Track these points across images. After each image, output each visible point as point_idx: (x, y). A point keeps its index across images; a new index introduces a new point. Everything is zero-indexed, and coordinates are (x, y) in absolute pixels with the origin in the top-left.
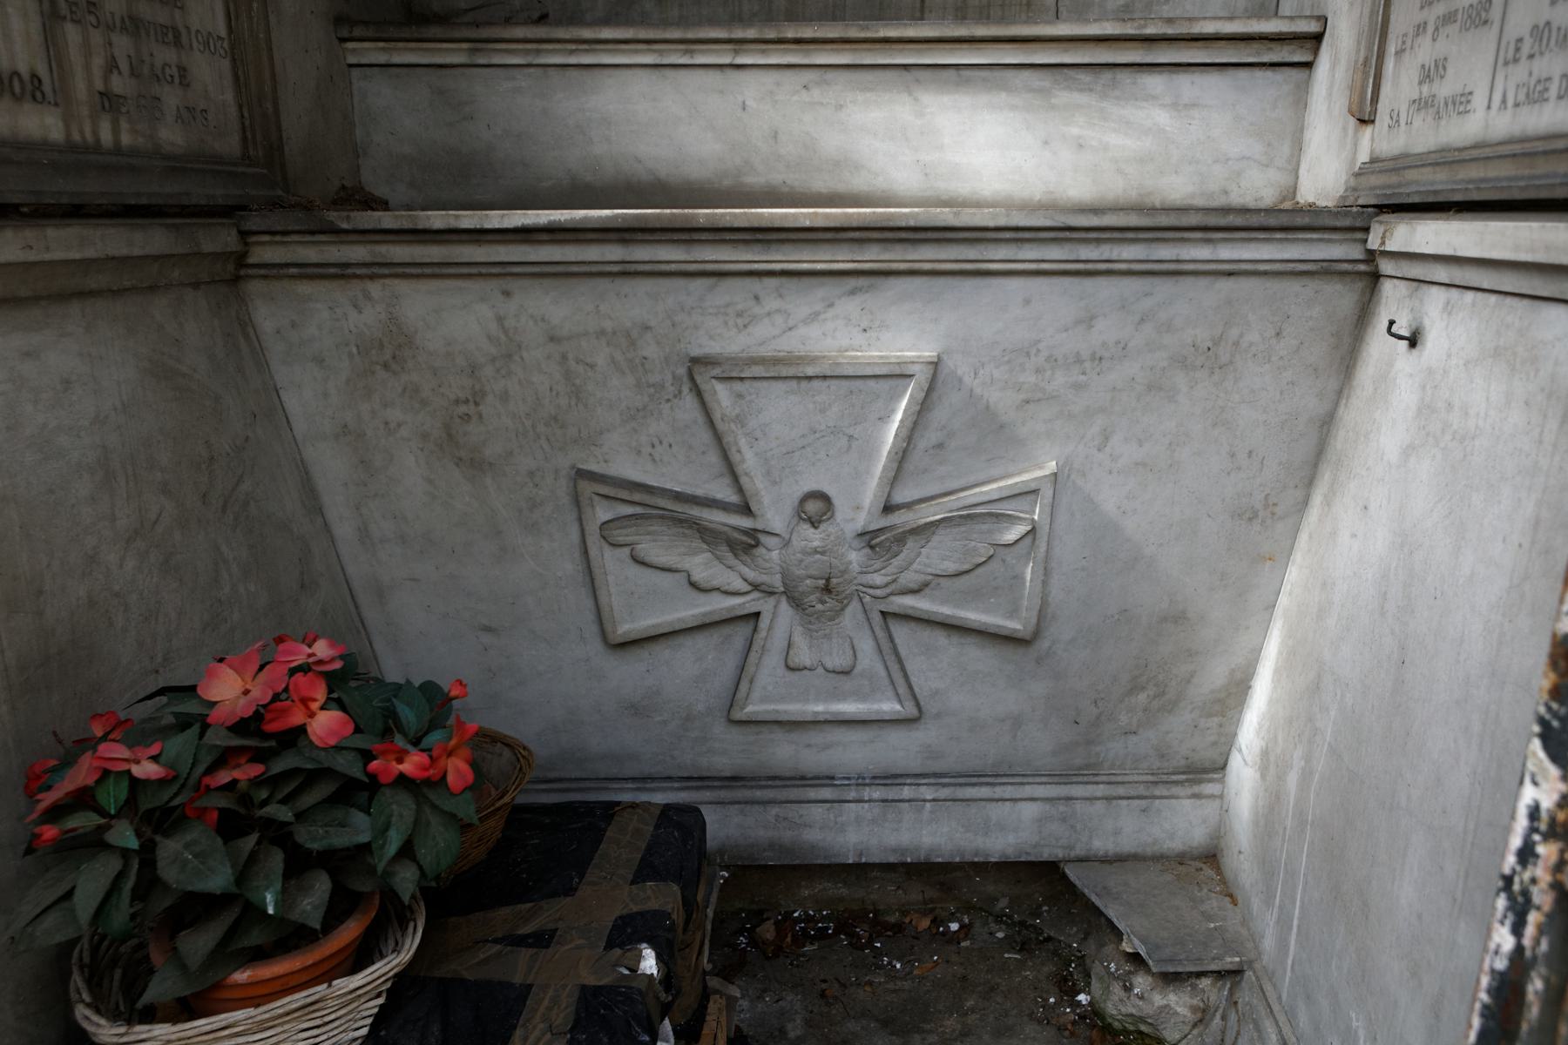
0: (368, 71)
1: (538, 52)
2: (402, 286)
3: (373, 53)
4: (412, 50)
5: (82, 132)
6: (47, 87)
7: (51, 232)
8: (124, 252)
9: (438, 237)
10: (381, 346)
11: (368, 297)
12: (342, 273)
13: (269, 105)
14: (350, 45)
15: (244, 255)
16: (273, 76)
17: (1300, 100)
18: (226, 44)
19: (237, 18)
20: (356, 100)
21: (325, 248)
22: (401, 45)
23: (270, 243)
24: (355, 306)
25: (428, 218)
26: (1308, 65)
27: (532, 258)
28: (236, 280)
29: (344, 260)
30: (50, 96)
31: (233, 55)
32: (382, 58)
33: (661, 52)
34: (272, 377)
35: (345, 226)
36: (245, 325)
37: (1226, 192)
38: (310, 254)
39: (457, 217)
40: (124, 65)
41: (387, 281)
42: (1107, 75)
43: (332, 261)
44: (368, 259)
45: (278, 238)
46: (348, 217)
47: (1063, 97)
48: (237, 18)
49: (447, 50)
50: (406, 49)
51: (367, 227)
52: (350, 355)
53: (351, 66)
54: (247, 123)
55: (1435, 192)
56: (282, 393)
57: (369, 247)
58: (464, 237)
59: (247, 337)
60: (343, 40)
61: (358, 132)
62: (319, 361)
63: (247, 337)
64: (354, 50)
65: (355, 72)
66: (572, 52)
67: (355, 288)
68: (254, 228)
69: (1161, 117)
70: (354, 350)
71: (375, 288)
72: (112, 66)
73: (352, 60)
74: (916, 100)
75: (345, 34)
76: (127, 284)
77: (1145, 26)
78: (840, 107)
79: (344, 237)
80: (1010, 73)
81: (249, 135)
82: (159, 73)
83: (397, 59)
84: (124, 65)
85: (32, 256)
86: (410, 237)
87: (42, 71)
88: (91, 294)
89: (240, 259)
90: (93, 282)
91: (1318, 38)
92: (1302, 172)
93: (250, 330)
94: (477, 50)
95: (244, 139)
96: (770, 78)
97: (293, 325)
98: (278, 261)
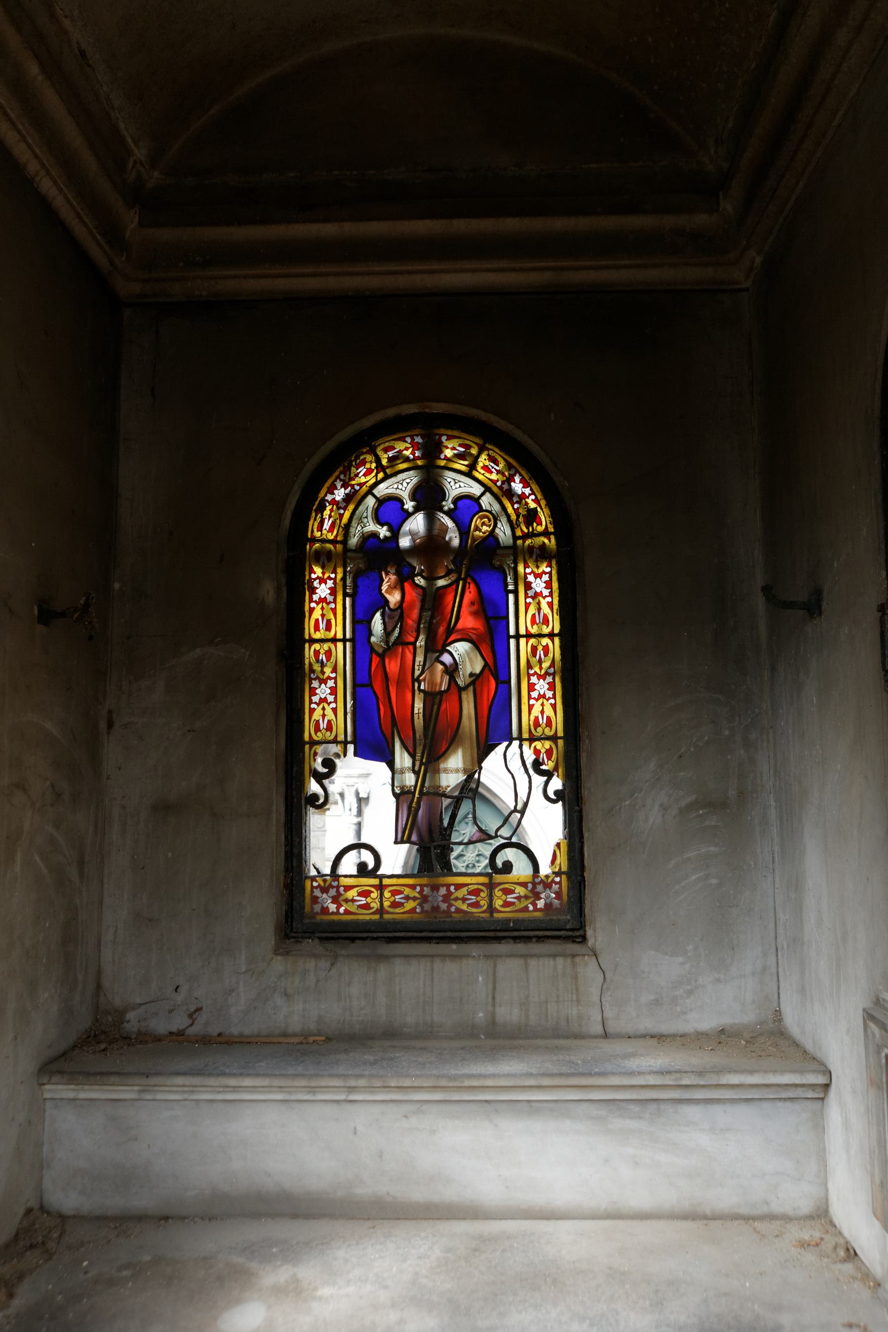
1: (192, 1092)
4: (94, 1090)
14: (47, 1087)
17: (819, 1125)
20: (47, 1123)
26: (822, 1099)
28: (799, 1180)
33: (289, 1093)
37: (767, 1203)
42: (653, 1107)
47: (618, 1123)
49: (122, 1091)
50: (90, 1090)
55: (454, 957)
60: (44, 1084)
61: (46, 1149)
64: (50, 1090)
66: (219, 1092)
69: (703, 1140)
73: (47, 1095)
74: (496, 1126)
77: (681, 1079)
78: (433, 1132)
80: (571, 1106)
91: (827, 1086)
92: (830, 1186)
96: (376, 1109)
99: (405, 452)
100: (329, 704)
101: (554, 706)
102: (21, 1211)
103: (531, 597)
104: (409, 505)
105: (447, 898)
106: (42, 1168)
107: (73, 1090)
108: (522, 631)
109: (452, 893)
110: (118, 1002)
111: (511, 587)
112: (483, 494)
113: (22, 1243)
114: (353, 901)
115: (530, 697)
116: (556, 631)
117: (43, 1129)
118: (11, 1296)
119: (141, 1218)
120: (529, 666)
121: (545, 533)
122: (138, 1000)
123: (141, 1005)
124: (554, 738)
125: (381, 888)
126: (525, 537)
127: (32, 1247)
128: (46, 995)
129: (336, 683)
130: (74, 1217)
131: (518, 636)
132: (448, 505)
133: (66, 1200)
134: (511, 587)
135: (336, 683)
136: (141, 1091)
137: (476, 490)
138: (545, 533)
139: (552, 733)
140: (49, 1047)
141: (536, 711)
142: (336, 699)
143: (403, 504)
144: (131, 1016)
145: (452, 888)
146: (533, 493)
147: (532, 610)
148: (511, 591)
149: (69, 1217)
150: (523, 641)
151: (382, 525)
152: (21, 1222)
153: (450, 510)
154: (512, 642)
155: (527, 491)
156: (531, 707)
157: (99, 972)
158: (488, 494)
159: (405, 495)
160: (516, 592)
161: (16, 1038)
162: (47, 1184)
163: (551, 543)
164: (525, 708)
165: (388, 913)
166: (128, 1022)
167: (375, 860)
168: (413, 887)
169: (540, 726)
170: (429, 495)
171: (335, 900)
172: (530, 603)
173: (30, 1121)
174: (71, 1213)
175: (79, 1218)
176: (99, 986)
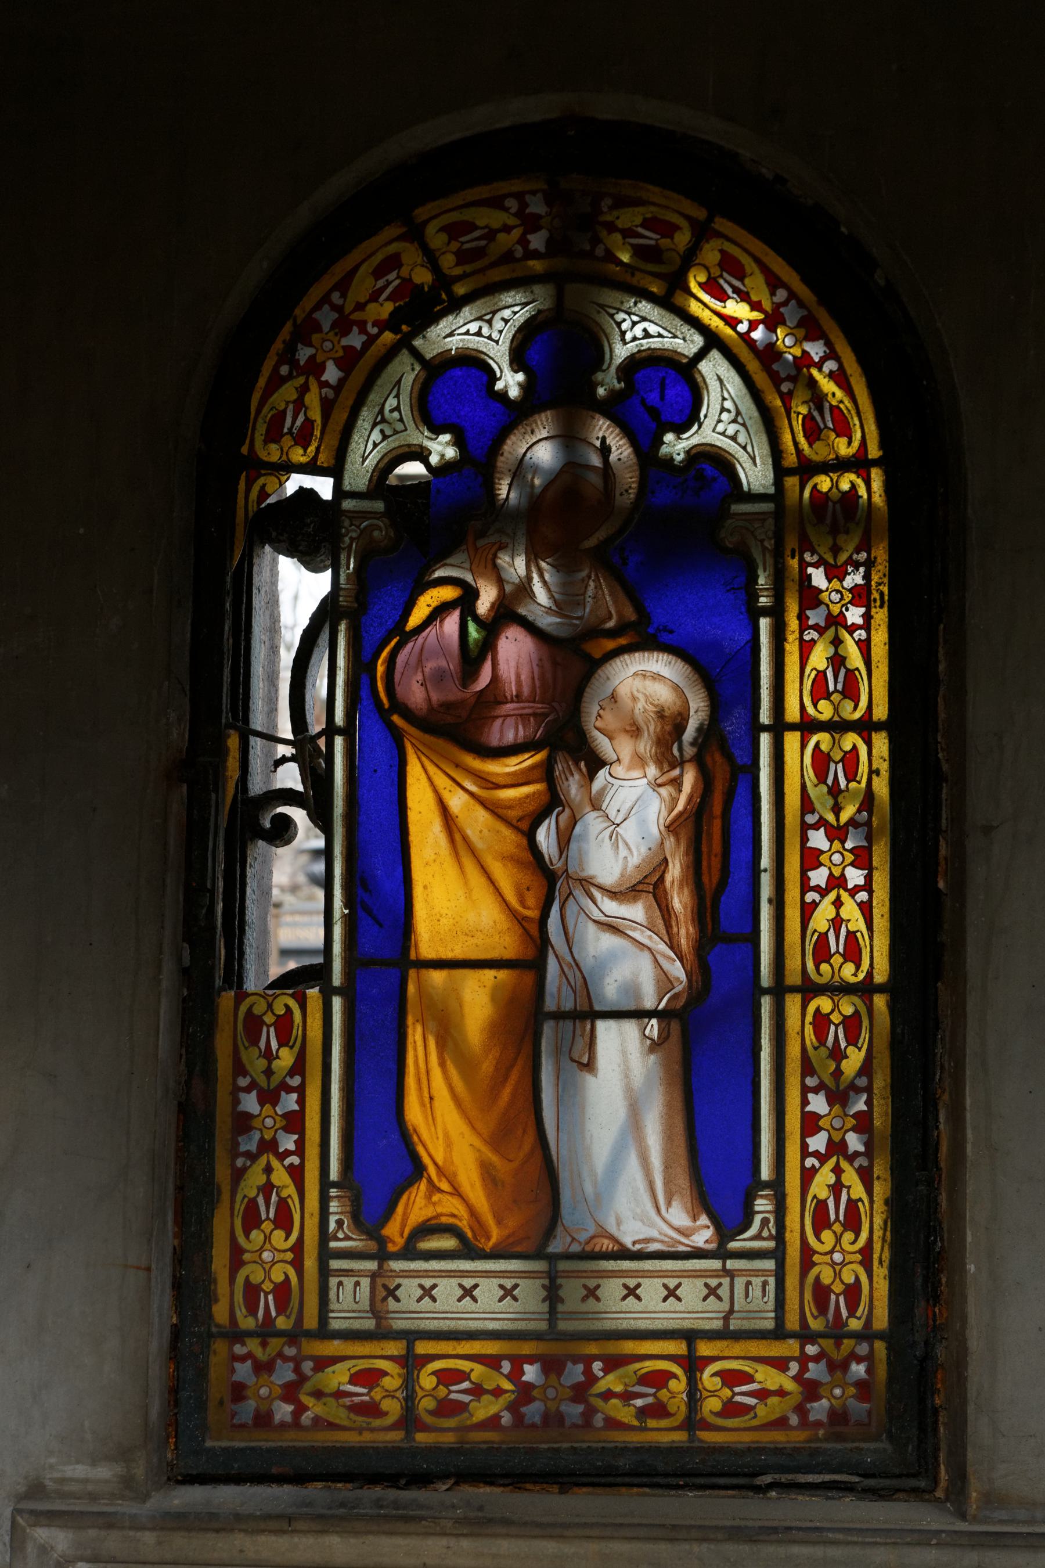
99: (501, 236)
100: (282, 1156)
101: (866, 909)
103: (816, 627)
104: (511, 382)
105: (580, 1392)
108: (793, 977)
109: (597, 1379)
111: (763, 601)
112: (701, 355)
114: (339, 1394)
115: (805, 886)
116: (881, 976)
120: (807, 805)
121: (859, 464)
124: (866, 989)
125: (411, 1363)
126: (807, 469)
129: (301, 1101)
131: (779, 728)
132: (607, 383)
134: (763, 601)
135: (301, 1101)
137: (689, 343)
138: (859, 464)
139: (857, 715)
141: (821, 920)
142: (300, 1145)
143: (493, 378)
145: (597, 1366)
146: (832, 354)
147: (819, 659)
148: (765, 612)
150: (792, 740)
151: (437, 430)
153: (612, 393)
154: (766, 1004)
155: (815, 350)
156: (807, 911)
158: (715, 354)
159: (498, 353)
160: (777, 613)
163: (872, 490)
164: (792, 649)
165: (425, 1428)
167: (396, 656)
168: (492, 1362)
169: (829, 1226)
170: (563, 357)
171: (290, 1393)
172: (813, 642)
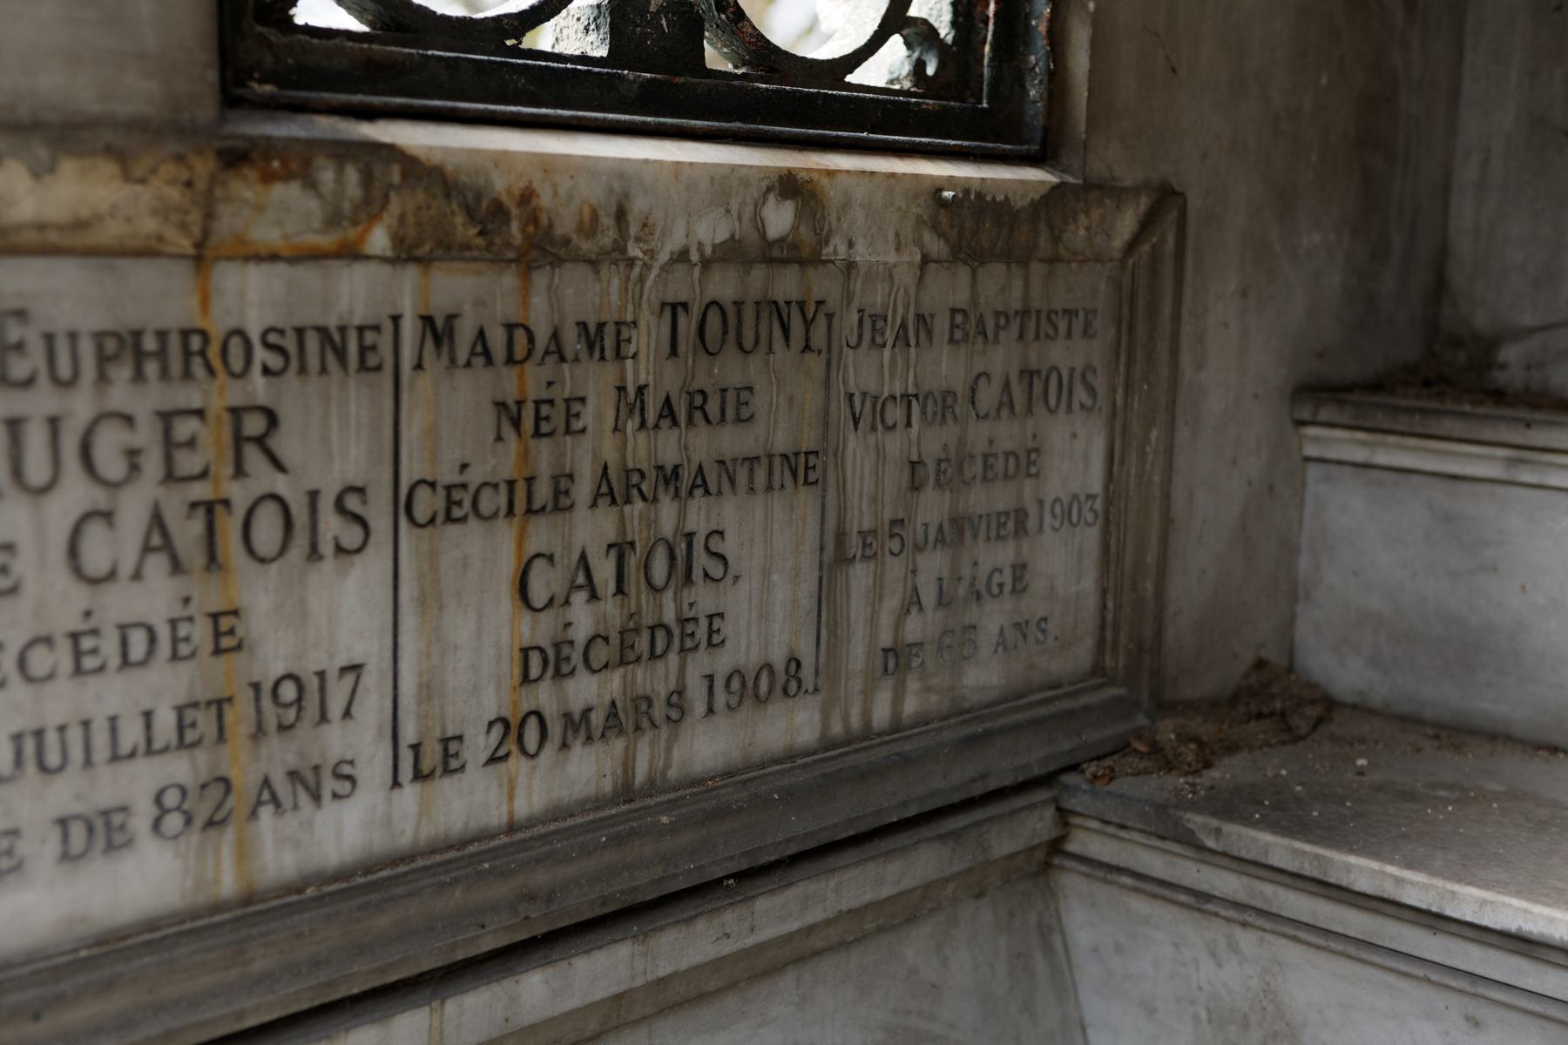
0: (1333, 468)
2: (1291, 952)
3: (1347, 446)
5: (846, 719)
6: (807, 672)
7: (762, 904)
8: (868, 897)
9: (1361, 901)
10: (1245, 1025)
11: (1234, 948)
12: (1201, 902)
13: (1149, 586)
14: (1311, 431)
15: (1062, 839)
16: (1167, 522)
18: (1098, 505)
19: (1122, 462)
20: (1308, 510)
21: (1179, 861)
22: (1391, 439)
23: (1101, 832)
24: (1213, 954)
25: (1348, 868)
27: (1531, 983)
29: (1204, 887)
30: (809, 683)
31: (1107, 523)
32: (1360, 455)
34: (1078, 1006)
35: (1210, 843)
36: (1049, 933)
38: (1155, 863)
39: (1399, 881)
40: (929, 597)
41: (1268, 937)
43: (1185, 883)
44: (1242, 897)
45: (1111, 829)
46: (1218, 831)
48: (1122, 462)
49: (1469, 456)
51: (1244, 854)
52: (1196, 1019)
53: (1308, 459)
54: (1110, 617)
56: (1090, 1031)
57: (1245, 879)
58: (1407, 914)
59: (1048, 949)
60: (1303, 423)
61: (1304, 562)
62: (1150, 1010)
63: (1048, 949)
65: (1314, 471)
67: (1216, 931)
68: (1079, 809)
70: (1203, 1014)
71: (1247, 940)
72: (913, 601)
73: (1311, 450)
75: (1306, 415)
76: (869, 926)
79: (1209, 857)
81: (1109, 635)
82: (981, 587)
83: (1382, 458)
84: (929, 597)
85: (727, 948)
86: (1316, 888)
87: (806, 653)
88: (817, 953)
89: (1056, 847)
90: (818, 942)
93: (1057, 940)
94: (1522, 461)
95: (1101, 642)
97: (1118, 949)
98: (1106, 859)
102: (1248, 657)
106: (1293, 597)
107: (1364, 443)
110: (1481, 320)
113: (1242, 709)
117: (1301, 522)
118: (1208, 765)
119: (1497, 737)
122: (1528, 320)
123: (1532, 331)
127: (1260, 716)
128: (1317, 238)
130: (1354, 707)
133: (1342, 670)
136: (1512, 462)
140: (1320, 355)
144: (1510, 354)
149: (1343, 705)
152: (1246, 676)
157: (1443, 253)
161: (1244, 294)
162: (1304, 632)
166: (1503, 366)
173: (1271, 488)
174: (1350, 699)
175: (1362, 709)
176: (1440, 286)
